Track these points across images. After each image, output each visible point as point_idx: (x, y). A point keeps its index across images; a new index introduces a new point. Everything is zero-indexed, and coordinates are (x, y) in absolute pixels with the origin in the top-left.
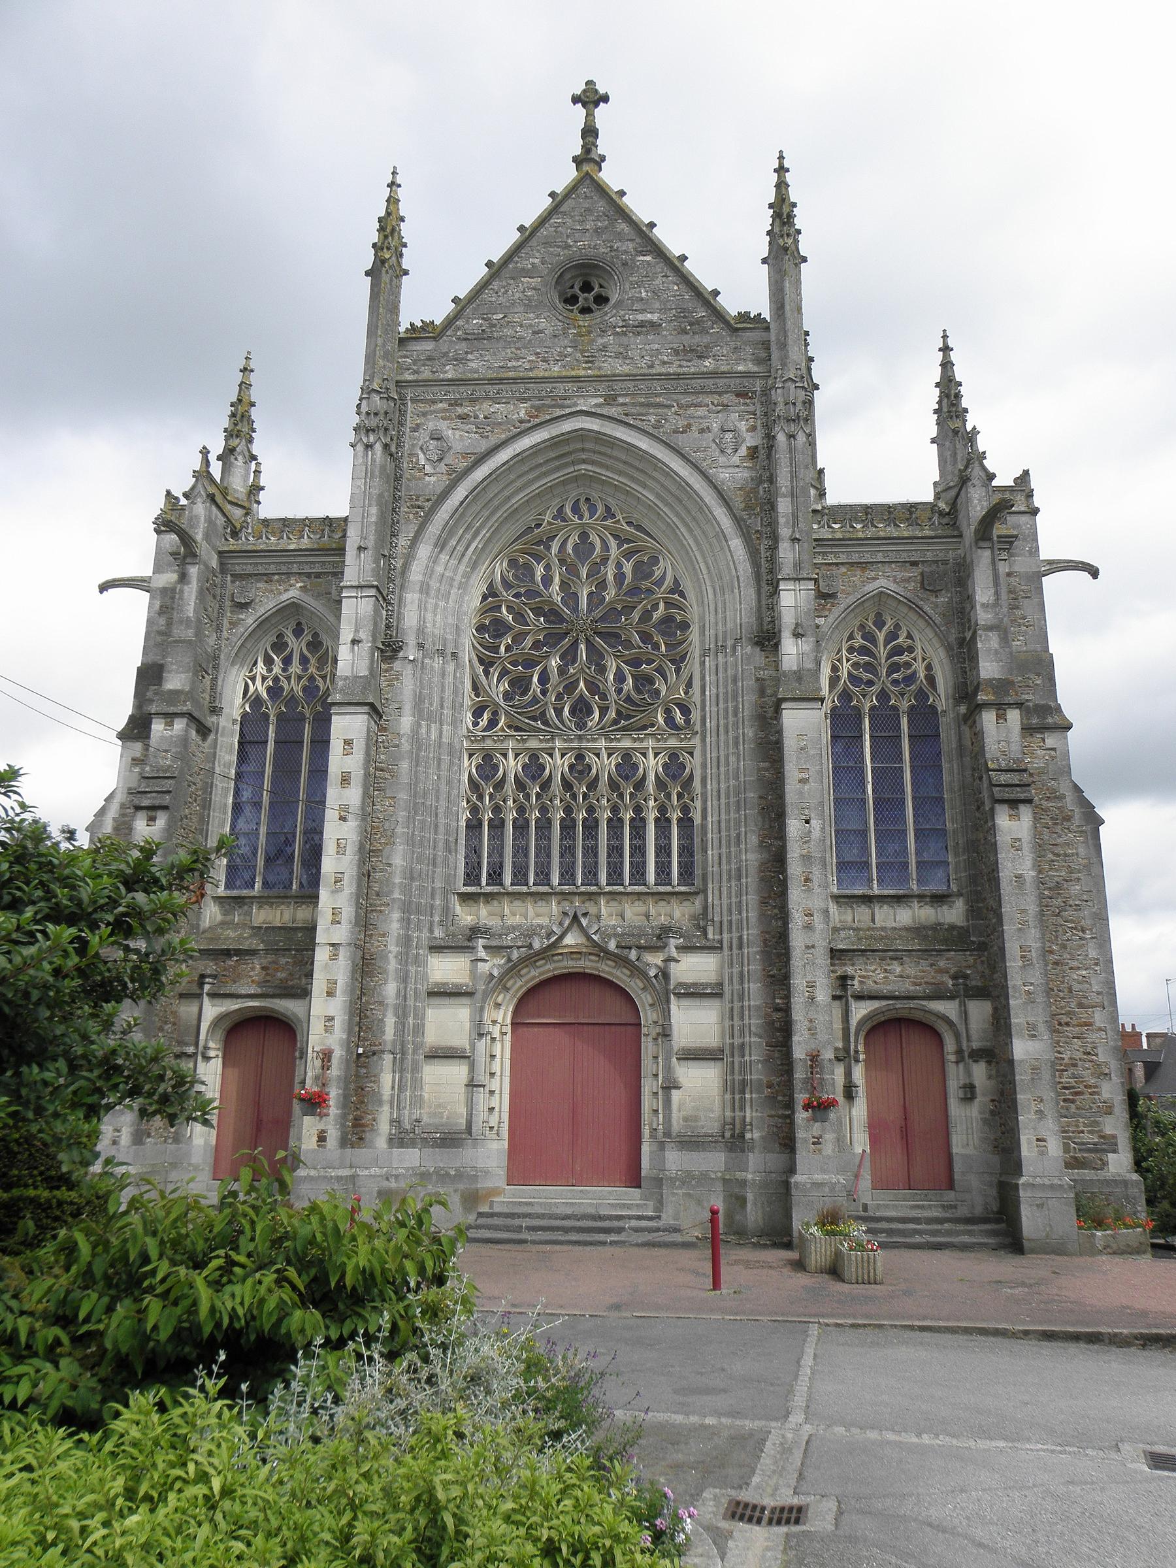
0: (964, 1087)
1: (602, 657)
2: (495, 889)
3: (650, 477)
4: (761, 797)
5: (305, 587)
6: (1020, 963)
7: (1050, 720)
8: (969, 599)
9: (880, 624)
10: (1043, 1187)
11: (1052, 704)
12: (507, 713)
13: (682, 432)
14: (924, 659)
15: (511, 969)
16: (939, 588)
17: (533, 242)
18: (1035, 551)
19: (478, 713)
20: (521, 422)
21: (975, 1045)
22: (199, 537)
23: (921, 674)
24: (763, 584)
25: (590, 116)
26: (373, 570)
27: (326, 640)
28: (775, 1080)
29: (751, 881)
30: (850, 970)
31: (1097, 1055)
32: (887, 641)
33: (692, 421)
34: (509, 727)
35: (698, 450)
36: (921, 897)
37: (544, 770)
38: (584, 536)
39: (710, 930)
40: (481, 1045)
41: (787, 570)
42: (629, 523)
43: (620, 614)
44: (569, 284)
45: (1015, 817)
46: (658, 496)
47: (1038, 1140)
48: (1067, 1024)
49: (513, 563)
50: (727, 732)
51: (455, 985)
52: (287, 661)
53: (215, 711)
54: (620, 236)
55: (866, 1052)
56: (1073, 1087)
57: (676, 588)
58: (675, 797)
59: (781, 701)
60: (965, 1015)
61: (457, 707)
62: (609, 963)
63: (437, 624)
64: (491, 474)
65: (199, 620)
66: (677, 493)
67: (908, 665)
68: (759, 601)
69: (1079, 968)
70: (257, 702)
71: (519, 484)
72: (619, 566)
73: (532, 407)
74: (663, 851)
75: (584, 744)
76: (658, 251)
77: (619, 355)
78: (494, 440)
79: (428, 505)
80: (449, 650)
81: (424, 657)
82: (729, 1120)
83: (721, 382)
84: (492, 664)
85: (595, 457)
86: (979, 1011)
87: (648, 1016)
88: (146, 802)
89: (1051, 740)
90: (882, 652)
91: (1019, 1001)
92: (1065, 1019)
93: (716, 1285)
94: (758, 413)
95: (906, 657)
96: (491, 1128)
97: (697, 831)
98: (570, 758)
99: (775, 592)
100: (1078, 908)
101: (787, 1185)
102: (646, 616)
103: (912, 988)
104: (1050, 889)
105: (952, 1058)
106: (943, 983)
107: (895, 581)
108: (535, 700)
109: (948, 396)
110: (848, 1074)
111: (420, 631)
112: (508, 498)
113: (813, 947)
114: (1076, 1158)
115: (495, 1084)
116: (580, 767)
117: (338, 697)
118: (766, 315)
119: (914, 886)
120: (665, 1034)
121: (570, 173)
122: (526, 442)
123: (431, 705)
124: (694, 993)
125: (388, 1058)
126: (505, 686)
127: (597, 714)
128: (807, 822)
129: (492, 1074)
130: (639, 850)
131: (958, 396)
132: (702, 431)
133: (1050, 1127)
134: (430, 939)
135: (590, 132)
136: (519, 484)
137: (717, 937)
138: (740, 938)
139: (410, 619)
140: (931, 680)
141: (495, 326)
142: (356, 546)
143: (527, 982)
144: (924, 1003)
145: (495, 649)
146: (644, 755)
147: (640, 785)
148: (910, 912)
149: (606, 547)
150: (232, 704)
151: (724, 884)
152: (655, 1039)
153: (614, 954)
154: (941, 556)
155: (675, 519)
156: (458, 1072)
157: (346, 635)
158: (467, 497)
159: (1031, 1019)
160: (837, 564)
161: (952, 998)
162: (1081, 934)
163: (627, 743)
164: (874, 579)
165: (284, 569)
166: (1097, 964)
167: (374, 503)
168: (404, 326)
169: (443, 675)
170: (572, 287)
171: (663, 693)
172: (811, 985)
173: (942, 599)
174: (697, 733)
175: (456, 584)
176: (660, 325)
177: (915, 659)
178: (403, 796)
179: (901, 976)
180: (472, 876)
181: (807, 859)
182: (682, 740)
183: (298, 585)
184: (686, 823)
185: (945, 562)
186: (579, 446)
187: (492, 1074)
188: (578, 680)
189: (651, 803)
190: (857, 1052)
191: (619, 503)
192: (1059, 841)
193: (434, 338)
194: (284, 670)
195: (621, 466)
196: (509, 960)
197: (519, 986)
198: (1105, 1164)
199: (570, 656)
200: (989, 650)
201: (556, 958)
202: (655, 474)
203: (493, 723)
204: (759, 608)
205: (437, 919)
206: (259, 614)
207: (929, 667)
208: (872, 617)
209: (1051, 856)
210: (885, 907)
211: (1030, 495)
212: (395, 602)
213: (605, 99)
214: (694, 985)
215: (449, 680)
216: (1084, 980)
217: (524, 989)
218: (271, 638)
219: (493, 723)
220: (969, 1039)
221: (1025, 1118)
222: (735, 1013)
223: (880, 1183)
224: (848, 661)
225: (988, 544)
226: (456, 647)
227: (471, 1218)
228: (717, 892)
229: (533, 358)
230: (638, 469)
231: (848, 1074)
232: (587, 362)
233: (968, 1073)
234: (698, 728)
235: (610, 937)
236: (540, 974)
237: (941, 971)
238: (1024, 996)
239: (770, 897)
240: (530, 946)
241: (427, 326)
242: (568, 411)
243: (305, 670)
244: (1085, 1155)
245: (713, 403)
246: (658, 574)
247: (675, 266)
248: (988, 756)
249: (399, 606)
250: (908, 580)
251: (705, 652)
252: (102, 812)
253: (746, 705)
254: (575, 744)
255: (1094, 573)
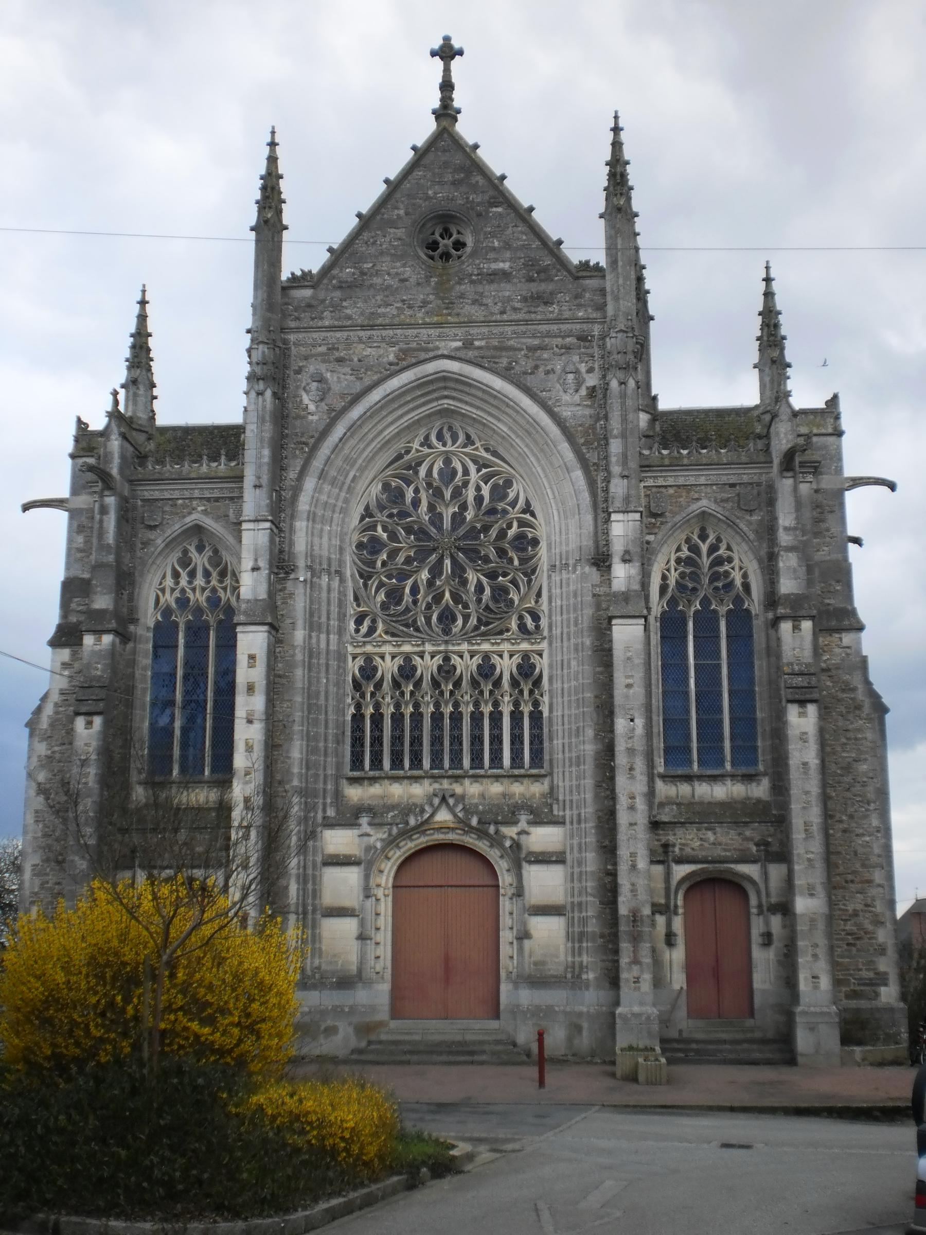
0: (763, 935)
1: (464, 571)
2: (376, 773)
3: (504, 412)
4: (596, 697)
5: (206, 510)
6: (804, 836)
7: (846, 623)
8: (774, 519)
9: (703, 537)
10: (815, 1014)
11: (849, 607)
12: (384, 622)
13: (530, 374)
14: (741, 568)
15: (391, 842)
16: (752, 508)
17: (398, 195)
18: (839, 470)
19: (359, 621)
20: (391, 364)
21: (773, 900)
22: (115, 472)
23: (738, 582)
24: (599, 511)
25: (447, 70)
26: (267, 506)
27: (226, 556)
28: (607, 931)
29: (589, 767)
30: (671, 838)
31: (875, 907)
32: (710, 553)
33: (539, 363)
34: (386, 633)
35: (544, 390)
36: (733, 776)
37: (416, 670)
38: (447, 461)
39: (555, 807)
40: (370, 903)
41: (618, 504)
42: (487, 450)
43: (480, 532)
44: (430, 232)
45: (802, 714)
46: (510, 428)
47: (813, 977)
48: (852, 881)
49: (386, 487)
50: (569, 639)
51: (345, 856)
52: (192, 575)
53: (135, 621)
54: (475, 188)
55: (685, 906)
56: (855, 934)
57: (528, 509)
58: (526, 693)
59: (610, 619)
60: (765, 875)
61: (342, 617)
62: (473, 835)
63: (325, 547)
64: (365, 413)
65: (118, 547)
66: (528, 426)
67: (727, 574)
68: (596, 526)
69: (863, 835)
70: (167, 612)
71: (390, 419)
72: (478, 489)
73: (401, 350)
74: (516, 739)
75: (451, 648)
76: (510, 203)
77: (475, 302)
78: (367, 381)
79: (312, 441)
80: (333, 569)
81: (312, 576)
82: (570, 964)
83: (564, 327)
84: (370, 578)
85: (454, 394)
86: (776, 871)
87: (506, 879)
88: (84, 709)
89: (847, 639)
90: (705, 561)
91: (802, 867)
92: (850, 877)
93: (542, 1083)
94: (596, 354)
95: (727, 567)
96: (378, 973)
97: (545, 722)
98: (438, 660)
99: (608, 521)
100: (864, 785)
101: (613, 1015)
102: (502, 534)
103: (723, 854)
104: (842, 768)
105: (754, 911)
106: (749, 849)
107: (715, 501)
108: (407, 610)
109: (768, 326)
110: (669, 924)
111: (310, 555)
112: (381, 431)
113: (636, 824)
114: (854, 991)
115: (380, 937)
116: (446, 669)
117: (242, 618)
118: (603, 263)
119: (728, 766)
120: (519, 893)
121: (430, 126)
122: (395, 383)
123: (320, 618)
124: (543, 859)
125: (292, 918)
126: (381, 597)
127: (460, 622)
128: (632, 720)
129: (378, 929)
130: (496, 740)
131: (777, 326)
132: (547, 373)
133: (822, 967)
134: (324, 818)
135: (447, 86)
136: (390, 419)
137: (561, 813)
138: (579, 815)
139: (300, 544)
140: (746, 587)
141: (365, 274)
142: (252, 484)
143: (405, 853)
144: (732, 866)
145: (372, 564)
146: (501, 656)
147: (497, 683)
148: (725, 789)
149: (466, 472)
150: (146, 615)
151: (567, 769)
152: (511, 899)
153: (477, 829)
154: (756, 479)
155: (526, 450)
156: (349, 926)
157: (247, 563)
158: (345, 434)
159: (811, 881)
160: (666, 487)
161: (754, 862)
162: (866, 806)
163: (486, 647)
164: (698, 499)
165: (187, 494)
166: (878, 831)
167: (266, 445)
168: (285, 275)
169: (329, 590)
170: (433, 234)
171: (516, 602)
172: (633, 855)
173: (755, 518)
174: (545, 638)
175: (338, 509)
176: (511, 273)
177: (733, 568)
178: (298, 699)
179: (714, 844)
180: (357, 762)
181: (631, 751)
182: (532, 644)
183: (200, 509)
184: (536, 717)
185: (759, 484)
186: (442, 384)
187: (378, 929)
188: (444, 592)
189: (507, 699)
190: (676, 906)
191: (478, 432)
192: (851, 727)
193: (312, 287)
194: (190, 582)
195: (480, 394)
196: (390, 835)
197: (398, 855)
198: (877, 995)
199: (436, 571)
200: (789, 568)
201: (428, 832)
202: (508, 410)
203: (372, 630)
204: (596, 533)
205: (329, 801)
206: (166, 535)
207: (745, 576)
208: (697, 531)
209: (844, 740)
210: (704, 784)
211: (837, 417)
212: (287, 529)
213: (460, 53)
214: (542, 853)
215: (335, 595)
216: (867, 845)
217: (403, 858)
218: (177, 554)
219: (372, 630)
220: (768, 895)
221: (802, 960)
222: (575, 877)
223: (692, 1013)
224: (676, 570)
225: (790, 474)
226: (340, 566)
227: (363, 1044)
228: (561, 775)
229: (399, 305)
230: (493, 405)
231: (669, 924)
232: (447, 308)
233: (767, 923)
234: (546, 633)
235: (472, 814)
236: (416, 846)
237: (747, 839)
238: (806, 863)
239: (603, 781)
240: (407, 823)
241: (306, 275)
242: (431, 354)
243: (208, 582)
244: (862, 988)
245: (557, 346)
246: (512, 495)
247: (524, 216)
248: (785, 661)
249: (291, 534)
250: (726, 500)
251: (553, 567)
252: (38, 711)
253: (585, 618)
254: (442, 648)
255: (892, 486)
